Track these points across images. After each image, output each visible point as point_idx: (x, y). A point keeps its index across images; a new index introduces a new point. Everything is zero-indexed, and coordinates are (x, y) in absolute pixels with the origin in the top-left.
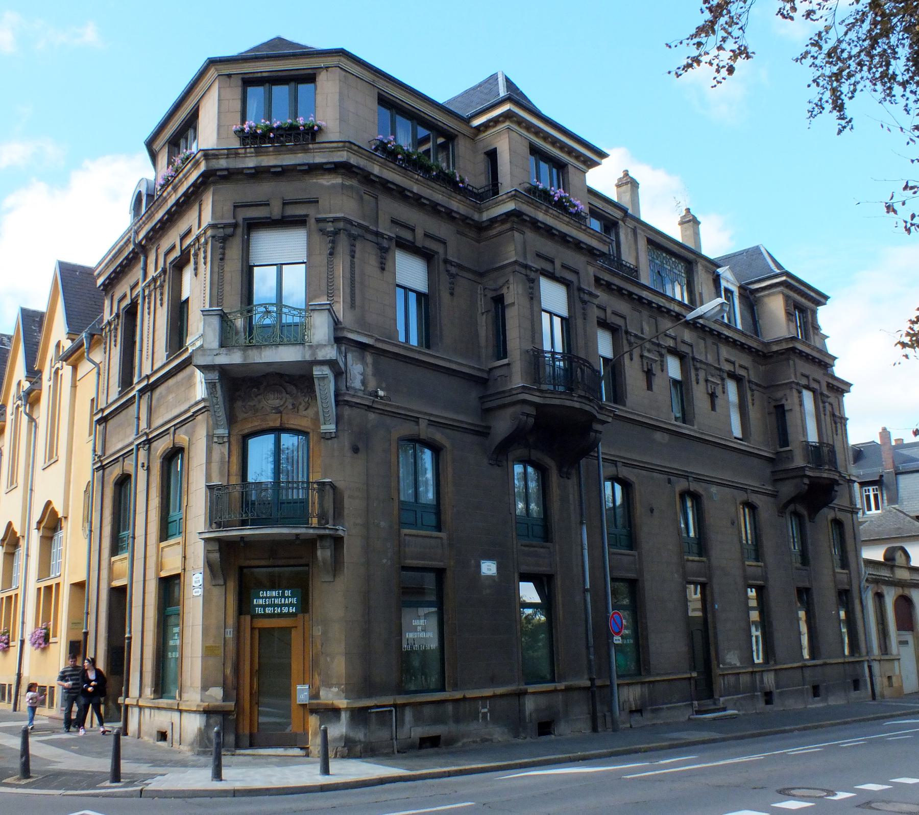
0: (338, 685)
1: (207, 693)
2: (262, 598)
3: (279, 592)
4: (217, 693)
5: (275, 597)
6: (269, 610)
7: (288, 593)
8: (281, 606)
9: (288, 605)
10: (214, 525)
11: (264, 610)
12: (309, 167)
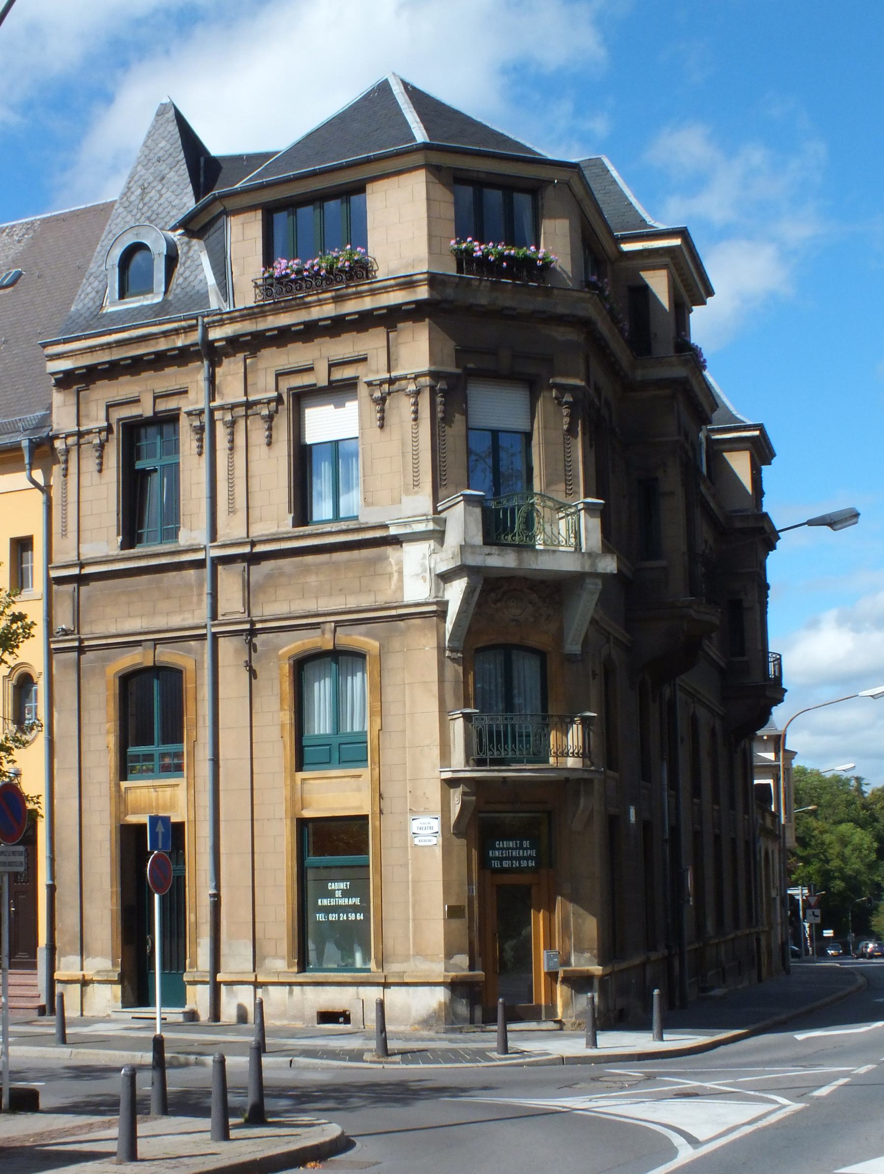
0: (590, 950)
1: (452, 961)
2: (499, 849)
3: (516, 843)
4: (463, 960)
5: (512, 849)
6: (506, 864)
7: (526, 844)
8: (519, 859)
9: (527, 858)
10: (471, 762)
11: (501, 864)
12: (226, 341)
